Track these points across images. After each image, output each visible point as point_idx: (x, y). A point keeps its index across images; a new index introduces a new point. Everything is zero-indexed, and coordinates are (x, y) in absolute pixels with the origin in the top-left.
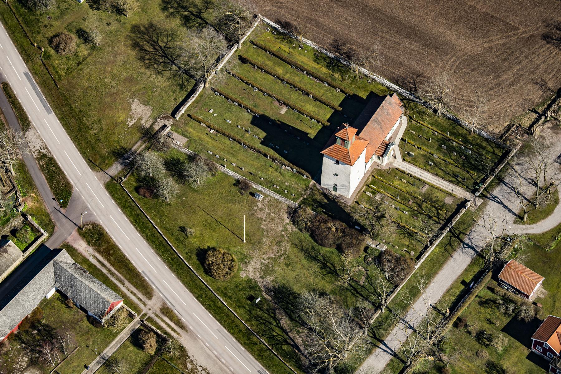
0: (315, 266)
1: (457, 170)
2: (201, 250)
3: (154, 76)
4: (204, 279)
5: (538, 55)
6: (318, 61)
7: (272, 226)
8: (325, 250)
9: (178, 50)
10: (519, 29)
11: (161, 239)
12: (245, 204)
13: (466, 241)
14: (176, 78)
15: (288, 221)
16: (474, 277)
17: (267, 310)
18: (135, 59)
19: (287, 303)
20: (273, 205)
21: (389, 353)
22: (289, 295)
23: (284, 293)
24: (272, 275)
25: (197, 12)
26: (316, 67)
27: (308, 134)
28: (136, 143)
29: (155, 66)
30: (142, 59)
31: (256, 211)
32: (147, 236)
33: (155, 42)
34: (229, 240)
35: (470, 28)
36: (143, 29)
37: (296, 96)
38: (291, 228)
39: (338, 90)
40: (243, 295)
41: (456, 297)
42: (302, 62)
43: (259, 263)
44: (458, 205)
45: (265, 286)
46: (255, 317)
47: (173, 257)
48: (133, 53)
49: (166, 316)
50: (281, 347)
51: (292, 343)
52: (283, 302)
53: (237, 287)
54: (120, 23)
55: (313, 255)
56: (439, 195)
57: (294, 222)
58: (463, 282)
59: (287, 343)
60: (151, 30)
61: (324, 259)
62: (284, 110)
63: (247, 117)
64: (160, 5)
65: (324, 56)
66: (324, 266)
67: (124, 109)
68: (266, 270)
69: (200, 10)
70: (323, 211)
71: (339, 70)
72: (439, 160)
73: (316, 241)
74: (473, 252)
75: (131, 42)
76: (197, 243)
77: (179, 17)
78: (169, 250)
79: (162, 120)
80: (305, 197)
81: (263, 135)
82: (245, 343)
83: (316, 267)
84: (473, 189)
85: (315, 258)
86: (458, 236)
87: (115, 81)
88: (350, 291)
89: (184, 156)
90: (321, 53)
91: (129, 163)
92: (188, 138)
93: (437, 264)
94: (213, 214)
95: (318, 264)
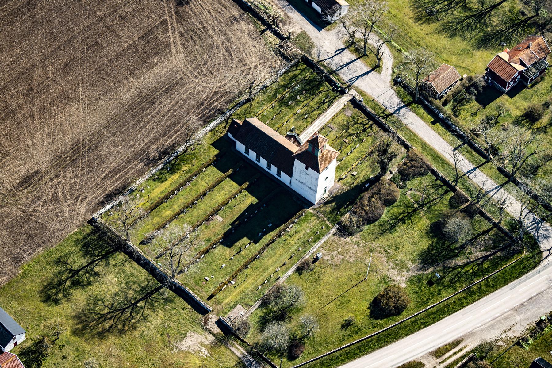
0: (401, 227)
1: (316, 100)
2: (370, 315)
3: (148, 324)
4: (405, 317)
5: (200, 14)
6: (163, 179)
7: (352, 252)
8: (384, 217)
9: (117, 298)
10: (166, 20)
11: (353, 347)
12: (323, 270)
13: (392, 111)
14: (156, 304)
15: (348, 239)
16: (429, 114)
17: (444, 273)
18: (121, 339)
19: (438, 256)
20: (328, 247)
21: (498, 191)
22: (429, 253)
23: (427, 256)
24: (406, 262)
25: (70, 273)
26: (170, 182)
27: (252, 204)
28: (233, 352)
29: (133, 321)
30: (122, 332)
31: (334, 263)
32: (348, 358)
33: (102, 317)
34: (362, 290)
35: (155, 54)
36: (80, 326)
37: (203, 205)
38: (356, 238)
39: (204, 169)
40: (425, 289)
41: (447, 132)
42: (161, 192)
43: (392, 270)
44: (354, 107)
45: (417, 270)
46: (451, 283)
47: (375, 340)
48: (112, 339)
49: (443, 355)
50: (486, 269)
51: (482, 260)
52: (437, 260)
53: (417, 293)
54: (66, 346)
55: (388, 227)
56: (340, 118)
57: (351, 234)
58: (433, 123)
59: (482, 263)
60: (83, 318)
61: (394, 219)
62: (218, 218)
63: (220, 249)
64: (49, 305)
65: (158, 173)
66: (403, 221)
67: (186, 357)
68: (401, 266)
69: (67, 269)
70: (345, 208)
71: (179, 165)
72: (303, 110)
73: (376, 220)
74: (404, 109)
75: (96, 339)
76: (362, 317)
77: (72, 291)
78: (367, 342)
79: (209, 324)
80: (326, 219)
81: (245, 240)
82: (479, 296)
83: (401, 227)
84: (338, 93)
85: (392, 226)
86: (386, 115)
87: (147, 360)
88: (432, 206)
89: (258, 311)
90: (154, 175)
91: (257, 361)
92: (237, 304)
93: (412, 137)
94: (330, 299)
95: (399, 224)
